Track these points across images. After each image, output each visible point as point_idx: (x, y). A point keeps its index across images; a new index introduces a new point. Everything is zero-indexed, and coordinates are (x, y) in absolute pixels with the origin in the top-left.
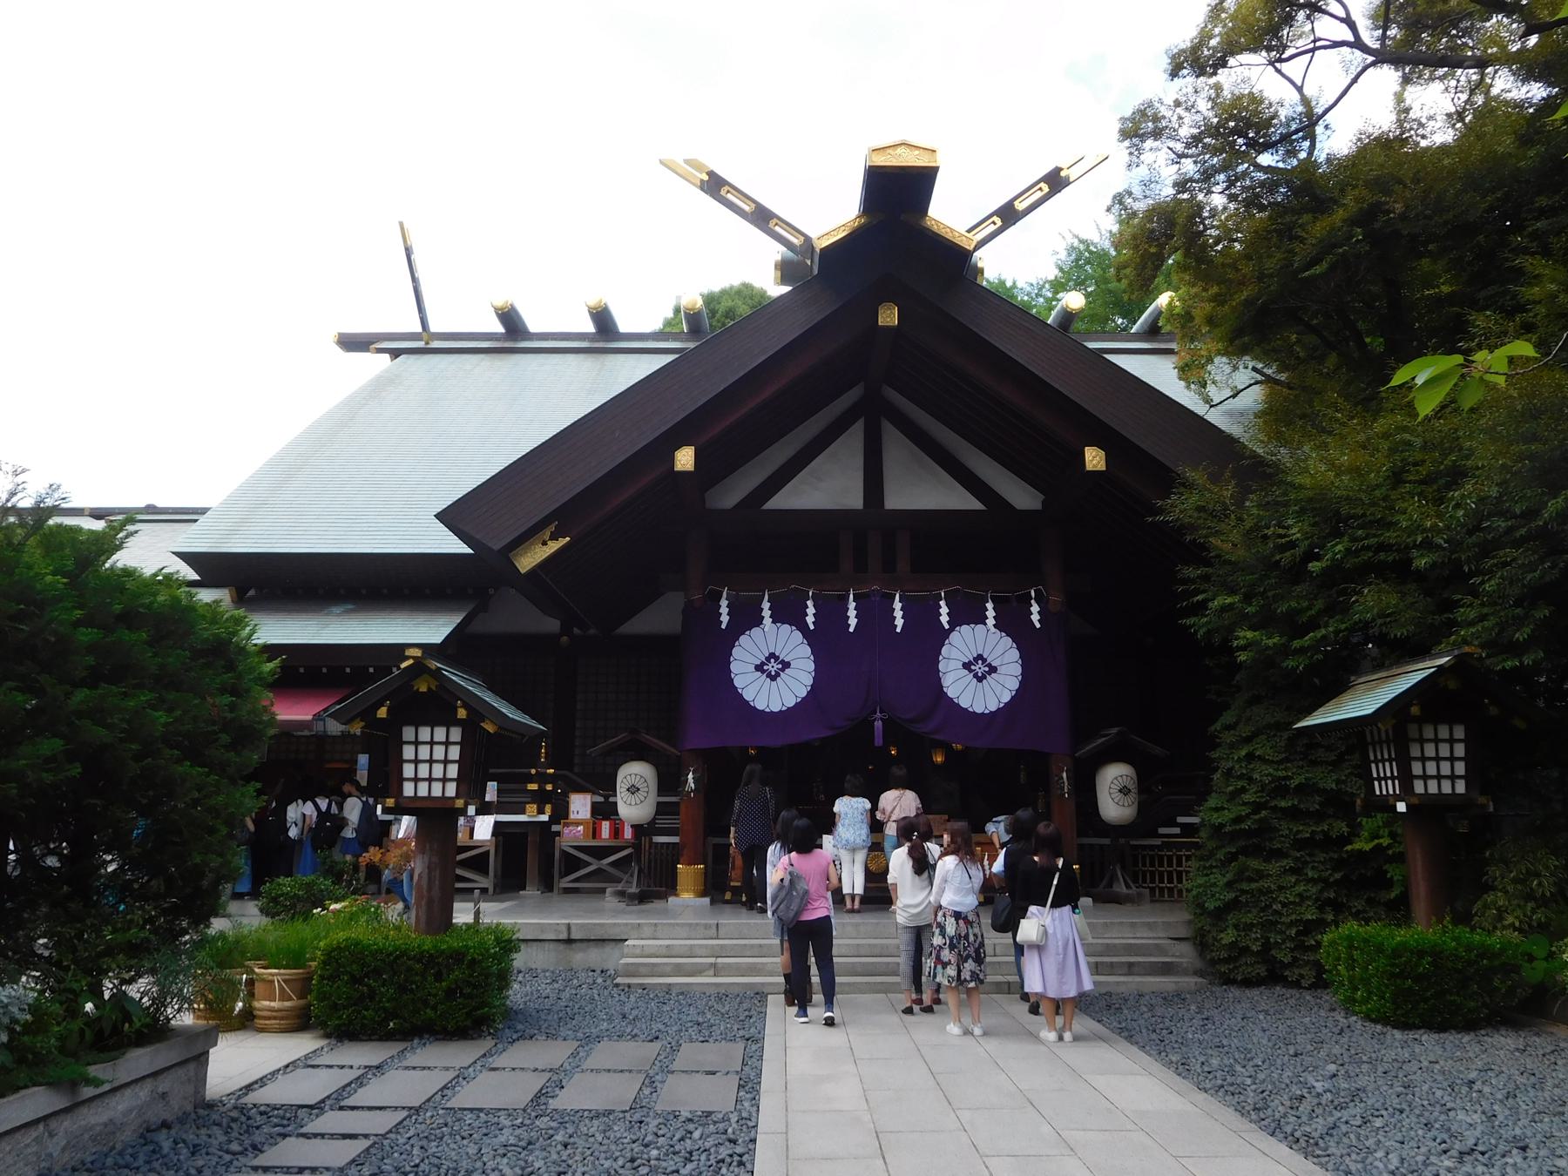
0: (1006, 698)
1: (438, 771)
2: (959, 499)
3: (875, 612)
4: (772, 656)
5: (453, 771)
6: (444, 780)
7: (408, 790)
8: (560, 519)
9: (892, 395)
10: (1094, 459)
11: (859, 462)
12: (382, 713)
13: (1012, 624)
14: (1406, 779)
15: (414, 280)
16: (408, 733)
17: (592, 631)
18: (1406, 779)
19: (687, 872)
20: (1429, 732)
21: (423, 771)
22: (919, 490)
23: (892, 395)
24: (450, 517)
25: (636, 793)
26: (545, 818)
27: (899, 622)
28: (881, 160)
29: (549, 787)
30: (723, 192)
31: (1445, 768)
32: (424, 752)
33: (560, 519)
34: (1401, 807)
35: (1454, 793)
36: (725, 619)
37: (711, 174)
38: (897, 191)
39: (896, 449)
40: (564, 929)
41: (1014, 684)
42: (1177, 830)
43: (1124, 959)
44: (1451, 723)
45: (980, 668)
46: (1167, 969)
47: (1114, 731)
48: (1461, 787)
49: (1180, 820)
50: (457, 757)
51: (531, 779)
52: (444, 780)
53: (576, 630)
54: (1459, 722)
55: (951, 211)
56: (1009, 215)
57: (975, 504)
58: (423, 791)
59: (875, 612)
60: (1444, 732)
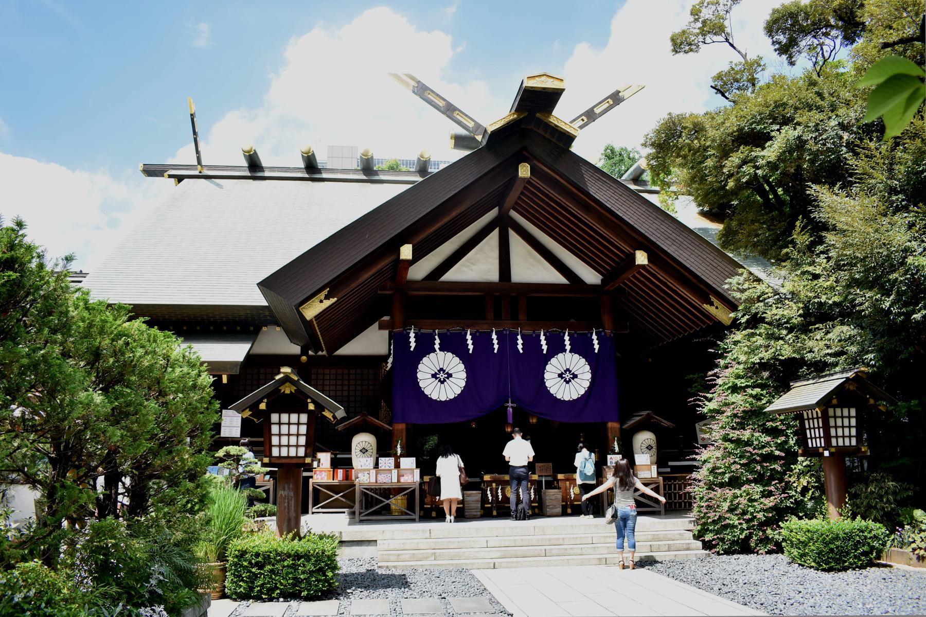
0: (458, 391)
1: (293, 440)
2: (553, 277)
3: (507, 341)
5: (302, 440)
6: (297, 446)
7: (275, 452)
8: (333, 287)
9: (514, 214)
11: (496, 254)
12: (263, 406)
13: (581, 348)
14: (828, 437)
15: (195, 133)
16: (274, 417)
18: (828, 437)
21: (284, 440)
22: (530, 269)
23: (514, 214)
24: (266, 285)
27: (471, 347)
30: (426, 94)
32: (284, 429)
34: (826, 453)
38: (536, 102)
39: (517, 243)
41: (587, 384)
42: (668, 470)
45: (568, 377)
47: (645, 413)
48: (854, 442)
49: (670, 463)
50: (305, 432)
52: (297, 446)
55: (563, 114)
56: (590, 116)
58: (284, 452)
59: (507, 341)
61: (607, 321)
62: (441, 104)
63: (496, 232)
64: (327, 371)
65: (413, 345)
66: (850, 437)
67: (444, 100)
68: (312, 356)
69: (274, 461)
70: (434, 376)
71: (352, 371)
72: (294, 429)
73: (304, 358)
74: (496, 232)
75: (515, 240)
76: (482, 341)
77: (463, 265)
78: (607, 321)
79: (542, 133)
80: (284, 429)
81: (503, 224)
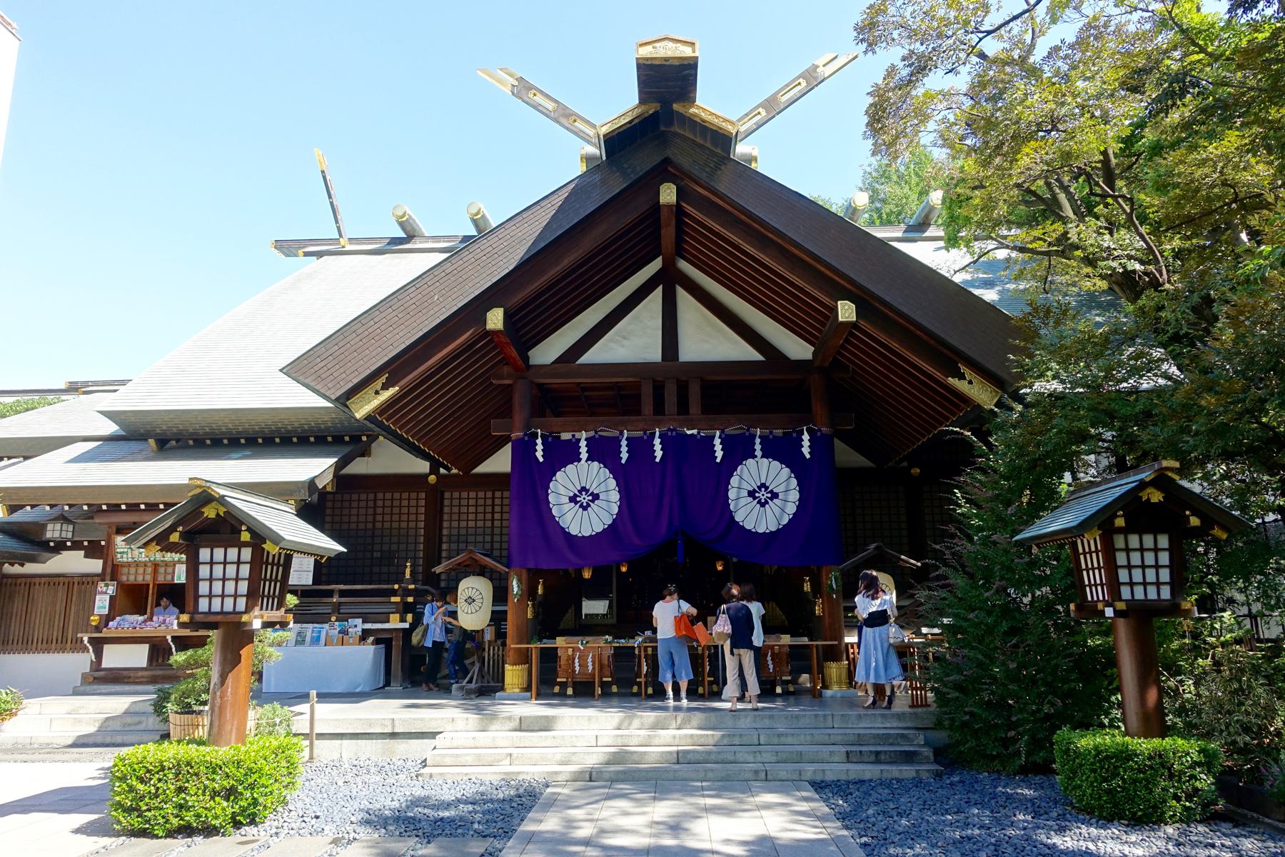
4: (583, 489)
7: (203, 605)
9: (684, 265)
10: (846, 311)
17: (454, 471)
19: (513, 675)
20: (1134, 541)
22: (704, 341)
23: (684, 265)
24: (297, 370)
25: (473, 605)
26: (406, 625)
28: (646, 52)
29: (410, 599)
31: (1151, 575)
33: (393, 369)
34: (1109, 612)
35: (1159, 599)
36: (719, 454)
37: (520, 79)
38: (668, 82)
40: (389, 723)
43: (872, 748)
44: (1155, 532)
45: (763, 496)
46: (909, 757)
48: (1166, 593)
51: (394, 593)
53: (442, 471)
54: (1162, 532)
55: (713, 101)
56: (773, 107)
57: (755, 356)
60: (1148, 540)
61: (818, 408)
62: (550, 105)
63: (658, 292)
64: (464, 495)
65: (719, 454)
66: (1158, 584)
67: (556, 102)
68: (444, 476)
69: (198, 618)
70: (573, 499)
71: (498, 494)
72: (1149, 558)
73: (432, 478)
74: (658, 292)
75: (685, 300)
76: (641, 447)
77: (611, 340)
78: (818, 408)
79: (691, 137)
80: (1136, 558)
81: (669, 280)
